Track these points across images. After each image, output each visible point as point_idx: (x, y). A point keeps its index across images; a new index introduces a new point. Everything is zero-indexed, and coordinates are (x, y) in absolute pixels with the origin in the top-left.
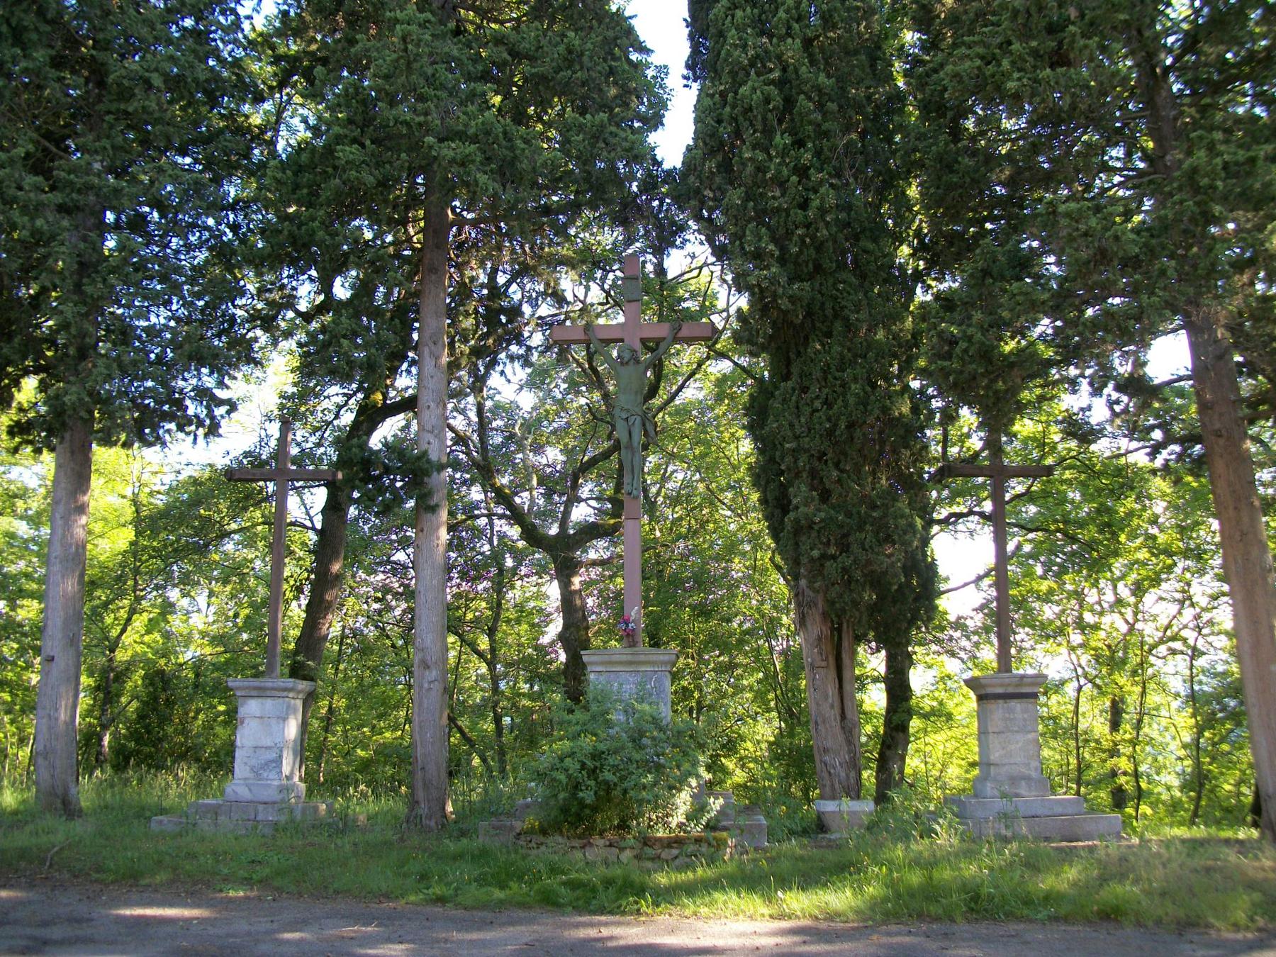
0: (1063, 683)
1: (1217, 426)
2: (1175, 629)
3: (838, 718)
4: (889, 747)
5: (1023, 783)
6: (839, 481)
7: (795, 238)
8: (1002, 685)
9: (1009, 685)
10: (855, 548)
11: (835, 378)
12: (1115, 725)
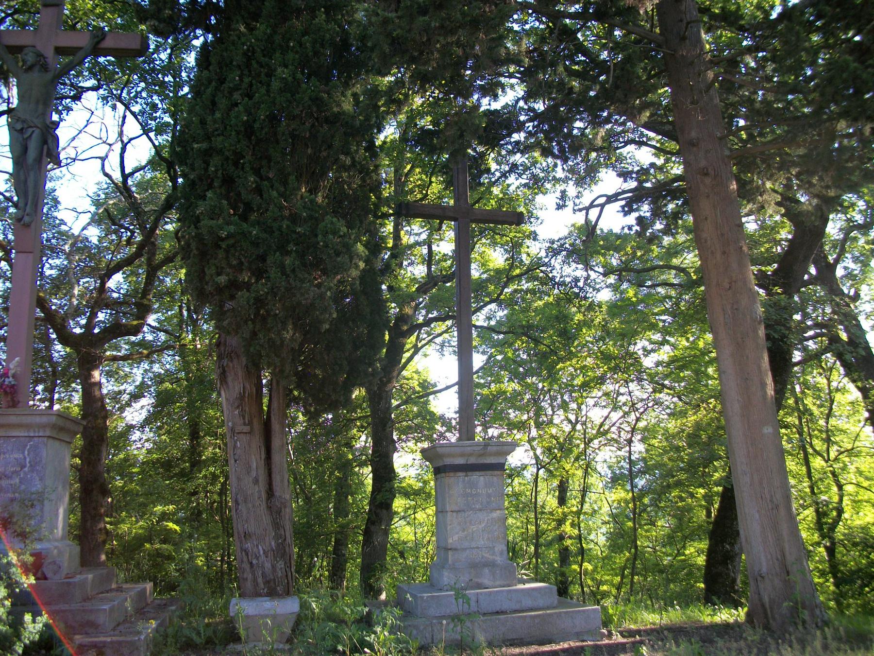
0: (524, 467)
1: (703, 163)
2: (606, 427)
3: (264, 495)
4: (373, 523)
5: (486, 570)
6: (259, 191)
8: (462, 455)
9: (471, 455)
10: (274, 273)
12: (562, 501)
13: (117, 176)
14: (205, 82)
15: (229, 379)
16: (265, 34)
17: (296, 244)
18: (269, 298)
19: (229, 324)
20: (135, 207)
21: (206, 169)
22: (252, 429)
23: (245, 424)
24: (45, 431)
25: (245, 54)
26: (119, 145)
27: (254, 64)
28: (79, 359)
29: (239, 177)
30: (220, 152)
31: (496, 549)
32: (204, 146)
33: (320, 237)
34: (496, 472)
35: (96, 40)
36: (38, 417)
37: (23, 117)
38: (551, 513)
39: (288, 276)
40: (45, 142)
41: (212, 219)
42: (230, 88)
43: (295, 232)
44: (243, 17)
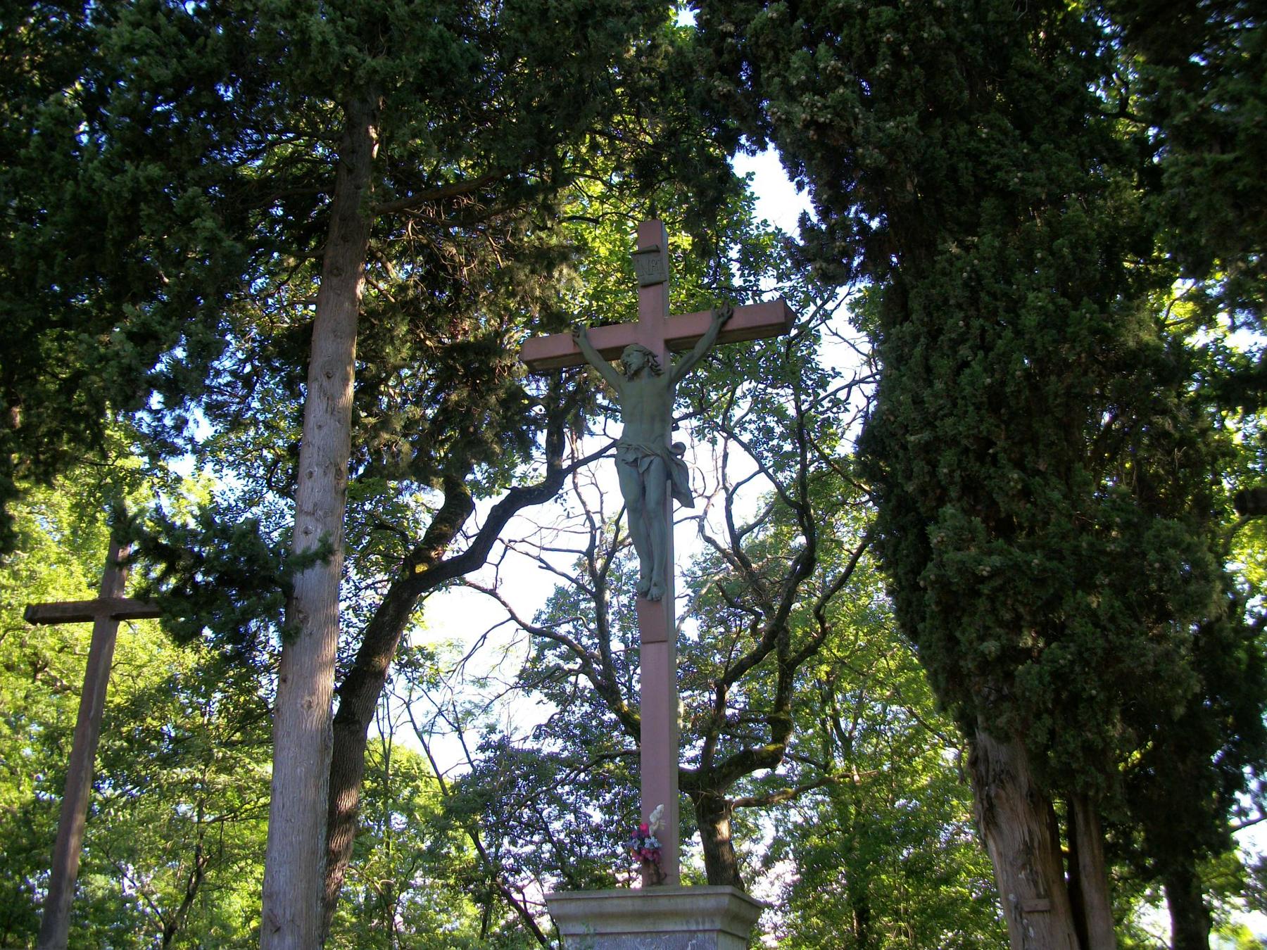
6: (1026, 493)
7: (884, 49)
11: (994, 296)
13: (724, 541)
14: (908, 339)
15: (1002, 819)
16: (993, 247)
17: (1108, 574)
18: (1077, 669)
19: (1010, 722)
20: (753, 580)
21: (933, 474)
22: (1052, 904)
23: (1039, 896)
24: (713, 922)
25: (966, 284)
26: (722, 494)
27: (984, 297)
28: (698, 808)
29: (990, 477)
30: (954, 441)
32: (926, 435)
33: (1152, 555)
35: (721, 320)
36: (701, 898)
37: (634, 444)
39: (1104, 629)
40: (669, 476)
41: (959, 550)
42: (951, 340)
43: (1103, 552)
44: (951, 232)
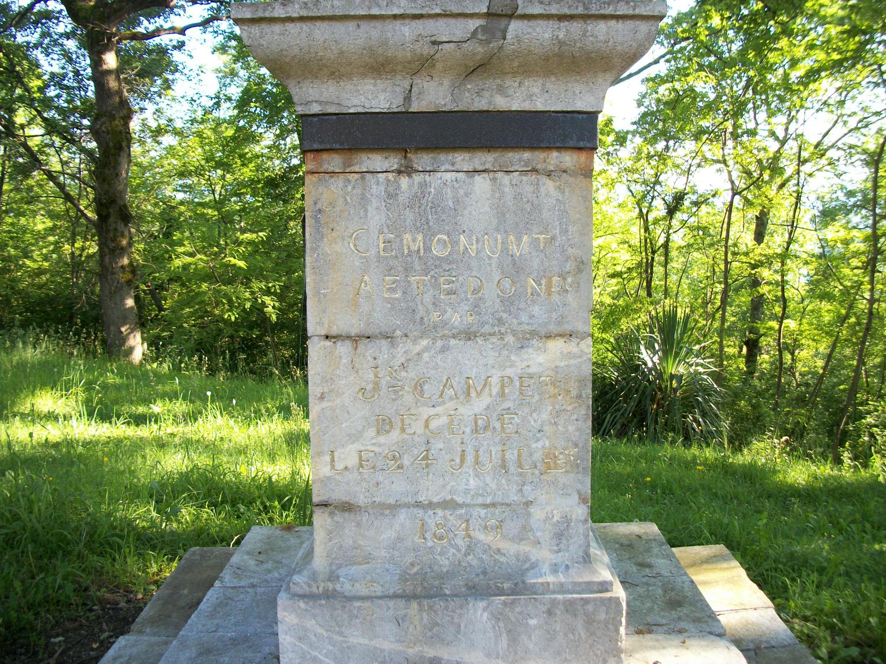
12: (759, 237)
31: (538, 514)
34: (554, 159)
38: (746, 254)
